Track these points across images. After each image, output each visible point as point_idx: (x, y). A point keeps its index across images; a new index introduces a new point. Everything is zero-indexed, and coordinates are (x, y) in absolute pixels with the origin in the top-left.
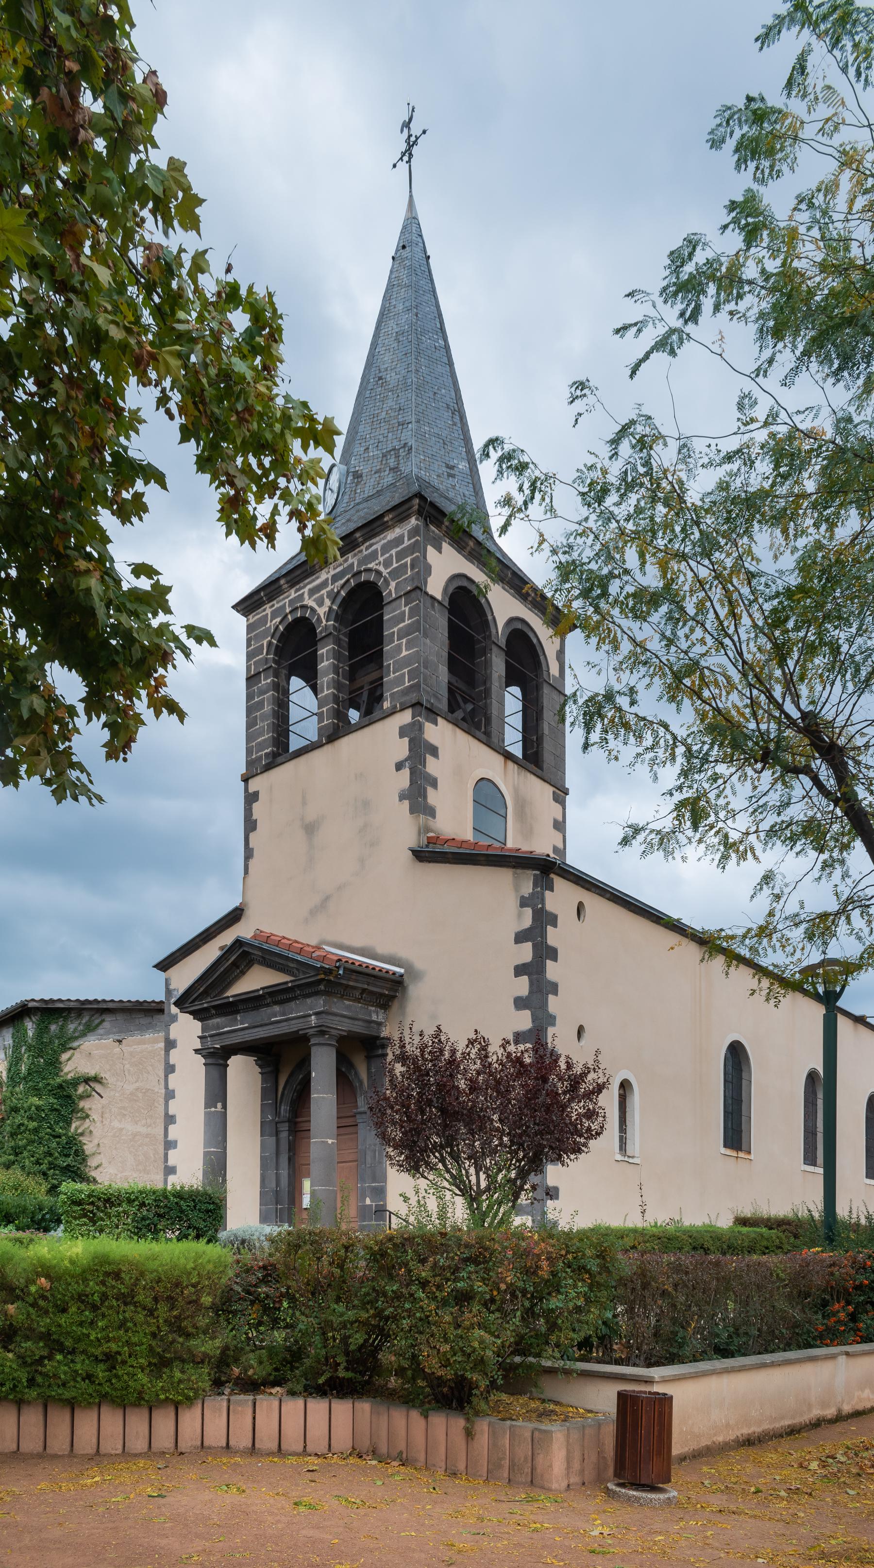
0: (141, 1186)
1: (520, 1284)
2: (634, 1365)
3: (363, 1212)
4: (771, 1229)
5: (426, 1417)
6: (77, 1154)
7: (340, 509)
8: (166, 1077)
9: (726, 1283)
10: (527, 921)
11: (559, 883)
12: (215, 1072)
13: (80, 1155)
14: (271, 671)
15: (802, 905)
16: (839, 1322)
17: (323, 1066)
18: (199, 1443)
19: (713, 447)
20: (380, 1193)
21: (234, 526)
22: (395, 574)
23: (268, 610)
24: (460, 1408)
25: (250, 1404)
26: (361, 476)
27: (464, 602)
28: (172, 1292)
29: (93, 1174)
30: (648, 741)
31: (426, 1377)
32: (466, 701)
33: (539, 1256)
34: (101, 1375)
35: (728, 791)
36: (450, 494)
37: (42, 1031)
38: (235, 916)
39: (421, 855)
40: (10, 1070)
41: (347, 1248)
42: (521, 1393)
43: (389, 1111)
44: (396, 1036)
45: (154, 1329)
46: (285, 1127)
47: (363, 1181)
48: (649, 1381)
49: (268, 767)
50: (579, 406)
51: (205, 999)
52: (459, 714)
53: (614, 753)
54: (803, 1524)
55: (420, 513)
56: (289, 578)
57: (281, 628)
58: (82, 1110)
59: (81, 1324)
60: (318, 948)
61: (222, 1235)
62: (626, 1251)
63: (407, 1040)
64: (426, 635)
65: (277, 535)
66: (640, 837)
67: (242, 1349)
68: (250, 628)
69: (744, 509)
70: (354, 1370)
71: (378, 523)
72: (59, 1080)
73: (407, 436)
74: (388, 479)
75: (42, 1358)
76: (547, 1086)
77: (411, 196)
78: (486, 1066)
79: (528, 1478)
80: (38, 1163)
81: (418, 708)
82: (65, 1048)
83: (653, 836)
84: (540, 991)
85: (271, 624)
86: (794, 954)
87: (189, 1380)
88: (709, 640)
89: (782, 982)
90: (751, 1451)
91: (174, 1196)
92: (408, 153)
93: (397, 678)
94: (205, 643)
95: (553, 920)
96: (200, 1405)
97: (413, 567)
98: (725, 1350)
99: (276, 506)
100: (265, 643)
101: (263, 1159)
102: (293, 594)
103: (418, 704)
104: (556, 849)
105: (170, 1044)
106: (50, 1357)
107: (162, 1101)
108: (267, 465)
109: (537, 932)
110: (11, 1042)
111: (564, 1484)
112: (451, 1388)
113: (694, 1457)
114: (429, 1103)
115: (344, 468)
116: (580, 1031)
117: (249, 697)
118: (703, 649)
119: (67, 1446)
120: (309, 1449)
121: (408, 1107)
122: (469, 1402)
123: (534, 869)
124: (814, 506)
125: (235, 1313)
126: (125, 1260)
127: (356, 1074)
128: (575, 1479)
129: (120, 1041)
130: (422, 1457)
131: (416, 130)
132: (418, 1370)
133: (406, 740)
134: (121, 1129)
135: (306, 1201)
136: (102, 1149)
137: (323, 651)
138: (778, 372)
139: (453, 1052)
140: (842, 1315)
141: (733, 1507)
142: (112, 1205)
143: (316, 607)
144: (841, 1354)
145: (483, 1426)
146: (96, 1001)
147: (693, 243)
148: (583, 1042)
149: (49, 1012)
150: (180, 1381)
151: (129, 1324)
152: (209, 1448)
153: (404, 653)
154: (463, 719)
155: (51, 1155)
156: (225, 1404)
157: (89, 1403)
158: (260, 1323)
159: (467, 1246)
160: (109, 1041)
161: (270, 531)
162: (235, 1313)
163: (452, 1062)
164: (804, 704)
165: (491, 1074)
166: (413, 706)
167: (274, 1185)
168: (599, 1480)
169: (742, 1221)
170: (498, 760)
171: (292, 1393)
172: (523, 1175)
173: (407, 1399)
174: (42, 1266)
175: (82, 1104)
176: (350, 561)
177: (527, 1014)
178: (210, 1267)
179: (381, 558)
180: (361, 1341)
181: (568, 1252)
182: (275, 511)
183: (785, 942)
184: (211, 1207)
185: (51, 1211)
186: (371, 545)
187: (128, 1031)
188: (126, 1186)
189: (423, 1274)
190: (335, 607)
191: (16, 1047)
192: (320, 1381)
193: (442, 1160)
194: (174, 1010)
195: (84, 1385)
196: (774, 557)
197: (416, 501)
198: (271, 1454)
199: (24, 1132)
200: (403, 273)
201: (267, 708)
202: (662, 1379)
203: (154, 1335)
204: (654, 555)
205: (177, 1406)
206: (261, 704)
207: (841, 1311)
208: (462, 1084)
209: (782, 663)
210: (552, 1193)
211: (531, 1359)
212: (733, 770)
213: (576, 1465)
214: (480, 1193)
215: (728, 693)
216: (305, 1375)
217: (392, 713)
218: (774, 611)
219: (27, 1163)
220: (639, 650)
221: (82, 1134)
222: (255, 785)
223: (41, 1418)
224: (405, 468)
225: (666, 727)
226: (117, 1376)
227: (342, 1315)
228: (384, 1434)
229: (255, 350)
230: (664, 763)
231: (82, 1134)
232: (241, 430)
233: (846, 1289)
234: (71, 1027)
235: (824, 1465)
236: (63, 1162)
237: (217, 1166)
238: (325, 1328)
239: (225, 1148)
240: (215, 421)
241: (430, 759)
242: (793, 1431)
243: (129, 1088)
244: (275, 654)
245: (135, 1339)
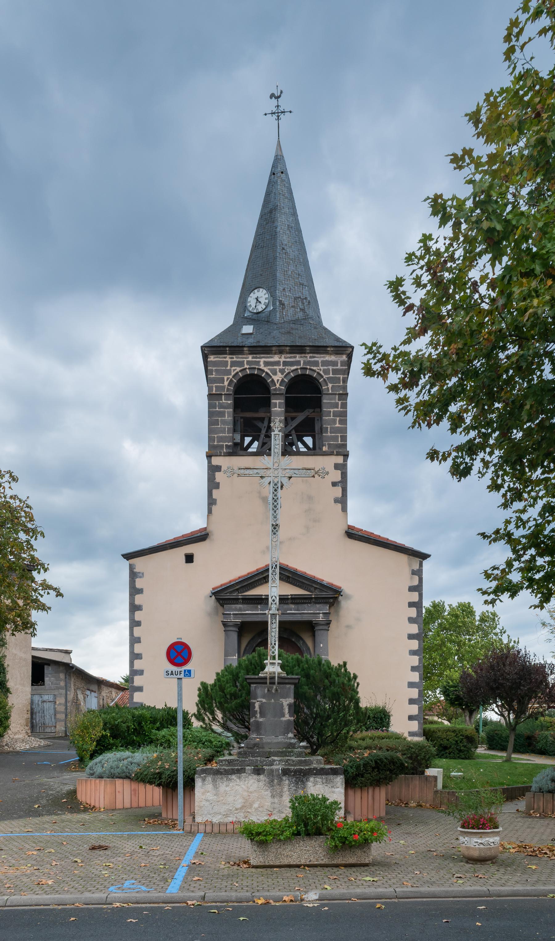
56: (251, 349)
71: (323, 349)
77: (279, 142)
127: (304, 642)
134: (16, 654)
176: (298, 359)
186: (314, 357)
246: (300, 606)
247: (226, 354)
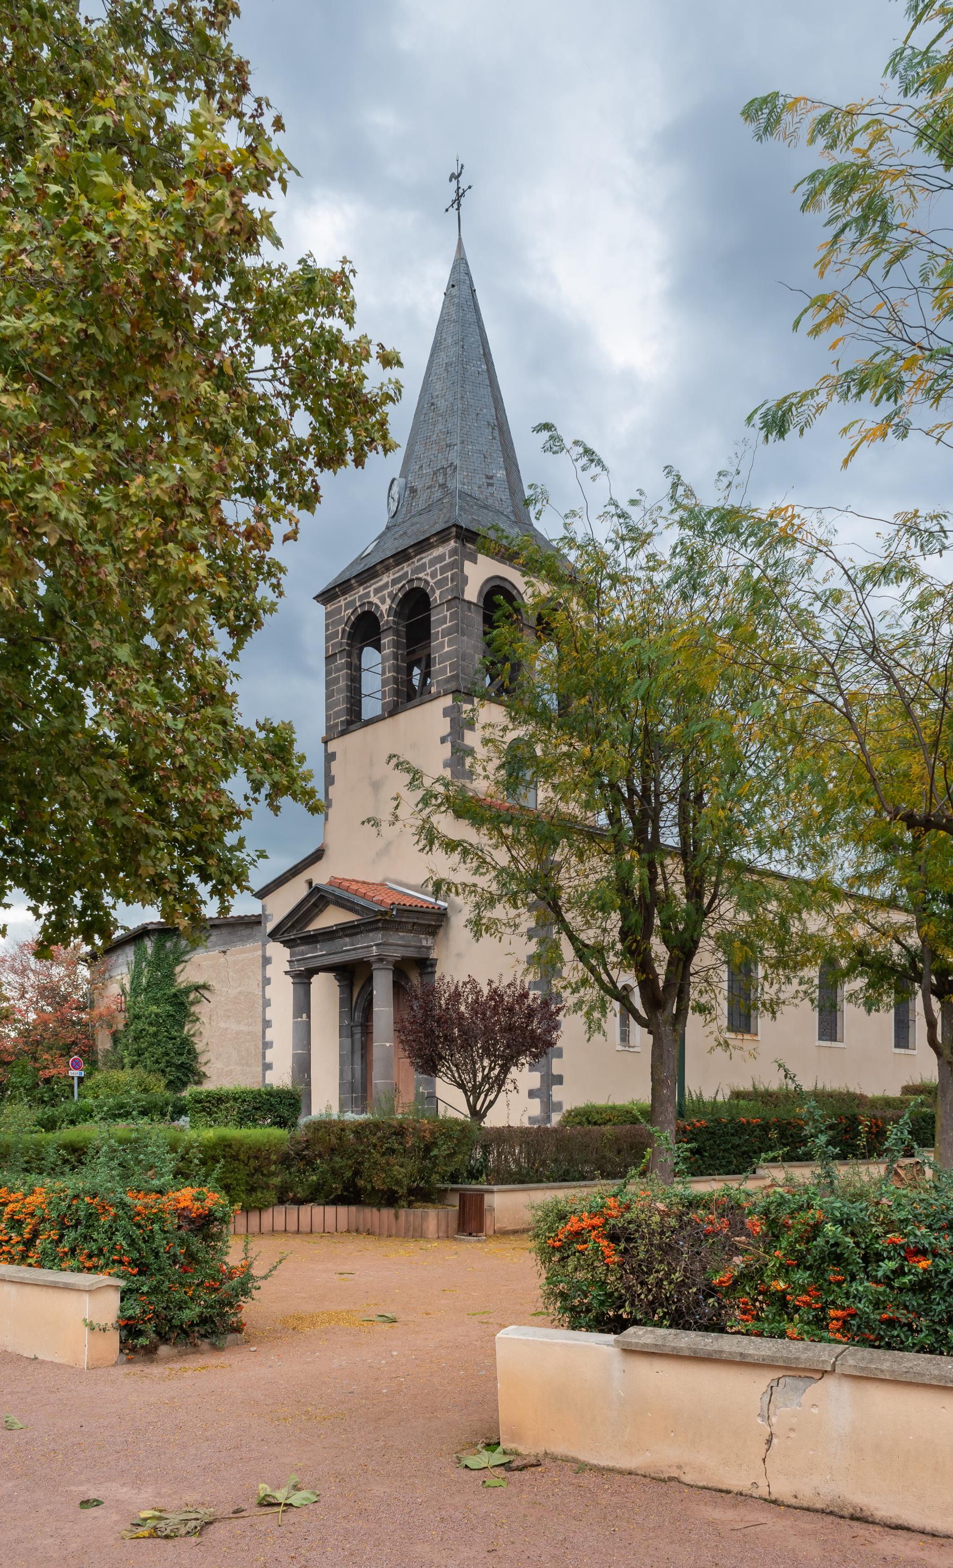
6: (189, 1052)
8: (263, 988)
12: (301, 989)
13: (193, 1054)
14: (345, 653)
22: (440, 584)
23: (342, 601)
26: (416, 491)
27: (497, 596)
29: (203, 1069)
37: (159, 948)
38: (318, 856)
40: (132, 982)
46: (358, 1030)
49: (343, 733)
55: (457, 537)
57: (353, 618)
58: (193, 1014)
64: (463, 634)
68: (328, 615)
72: (173, 990)
77: (460, 239)
80: (157, 1062)
81: (456, 694)
82: (178, 961)
93: (442, 669)
102: (361, 591)
117: (328, 673)
126: (234, 1139)
129: (224, 952)
136: (210, 1047)
155: (168, 1055)
160: (215, 953)
166: (453, 692)
167: (350, 1078)
169: (737, 1095)
175: (193, 1009)
179: (428, 570)
191: (138, 964)
197: (454, 529)
198: (307, 1233)
201: (342, 683)
205: (260, 1210)
206: (337, 680)
213: (443, 1227)
217: (438, 697)
221: (193, 1035)
222: (333, 746)
231: (193, 1035)
236: (178, 1060)
237: (303, 1066)
239: (309, 1050)
243: (233, 992)
247: (338, 596)
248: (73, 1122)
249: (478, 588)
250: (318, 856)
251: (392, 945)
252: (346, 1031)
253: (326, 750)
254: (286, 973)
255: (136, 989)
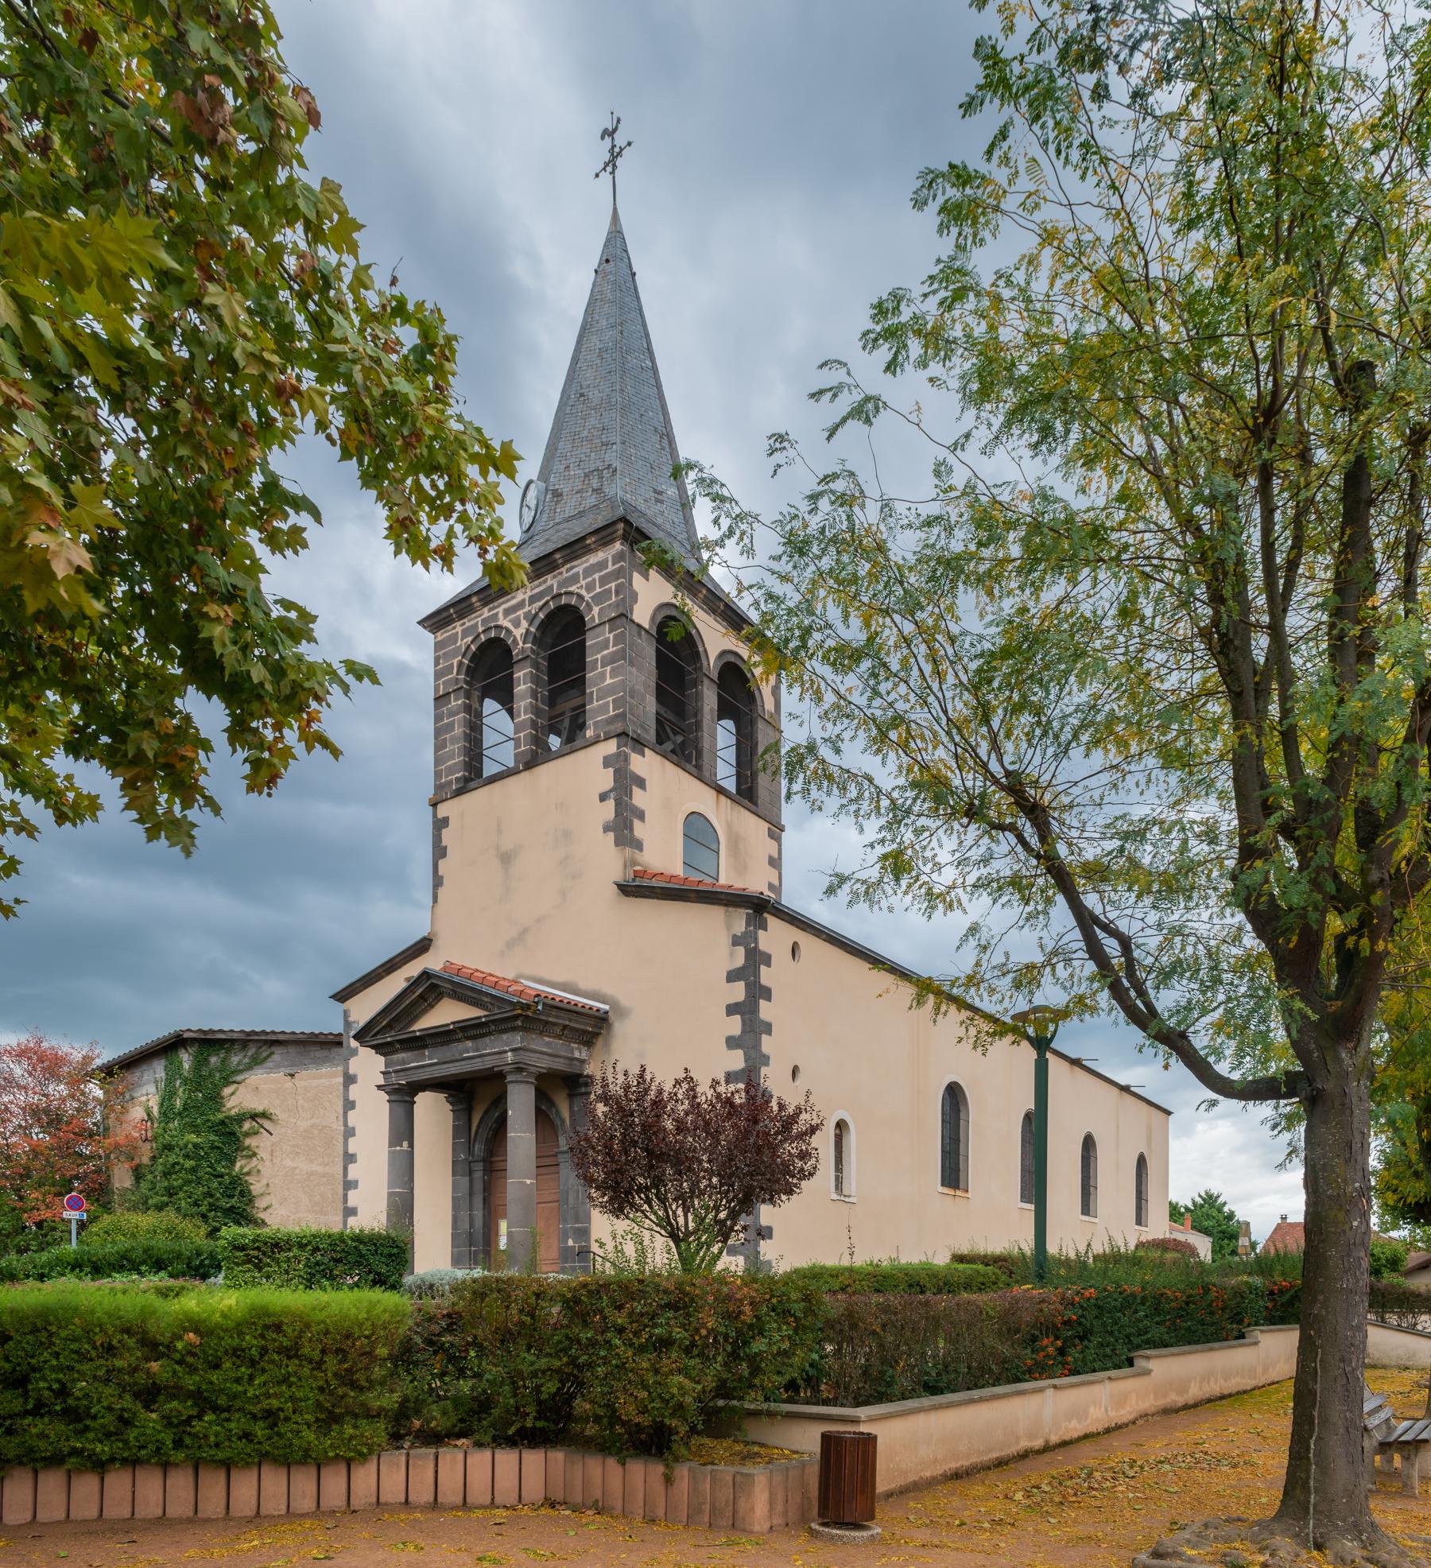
0: (314, 1229)
1: (722, 1329)
2: (842, 1405)
3: (565, 1254)
4: (987, 1265)
5: (624, 1464)
6: (242, 1194)
7: (538, 527)
9: (935, 1322)
10: (739, 960)
11: (772, 921)
12: (400, 1109)
13: (247, 1196)
14: (462, 693)
15: (1007, 955)
16: (1048, 1356)
17: (520, 1103)
18: (374, 1500)
19: (913, 511)
20: (584, 1233)
21: (405, 545)
22: (599, 599)
23: (458, 628)
24: (660, 1454)
25: (432, 1457)
28: (343, 1345)
29: (261, 1215)
30: (853, 792)
31: (624, 1424)
32: (675, 733)
33: (741, 1301)
34: (259, 1433)
35: (934, 844)
36: (658, 518)
37: (200, 1063)
38: (423, 946)
39: (627, 890)
41: (538, 1295)
42: (725, 1436)
43: (590, 1152)
44: (598, 1075)
45: (321, 1383)
46: (479, 1166)
47: (565, 1221)
48: (855, 1421)
49: (459, 792)
50: (779, 457)
51: (389, 1032)
52: (669, 746)
53: (818, 803)
54: (1004, 1554)
55: (625, 538)
57: (473, 648)
58: (248, 1148)
59: (238, 1380)
60: (516, 982)
61: (408, 1280)
62: (835, 1293)
63: (611, 1080)
64: (632, 664)
65: (455, 559)
66: (846, 888)
67: (424, 1400)
68: (438, 646)
69: (950, 569)
70: (547, 1419)
71: (580, 545)
72: (220, 1116)
73: (612, 457)
74: (591, 500)
75: (190, 1418)
76: (758, 1128)
77: (615, 209)
78: (695, 1106)
79: (729, 1521)
80: (196, 1204)
81: (624, 738)
83: (858, 885)
84: (753, 1031)
85: (462, 643)
86: (1008, 1003)
87: (362, 1435)
88: (912, 697)
89: (1000, 1028)
90: (958, 1484)
91: (353, 1240)
92: (611, 164)
94: (366, 680)
95: (767, 960)
96: (375, 1461)
97: (617, 593)
98: (934, 1387)
99: (451, 527)
100: (455, 662)
101: (455, 1201)
102: (486, 613)
103: (624, 734)
104: (771, 887)
105: (350, 1079)
106: (200, 1417)
107: (341, 1138)
108: (442, 487)
109: (751, 970)
110: (163, 1075)
111: (767, 1526)
112: (648, 1434)
113: (901, 1492)
114: (634, 1144)
115: (542, 485)
116: (795, 1071)
117: (438, 718)
118: (908, 706)
119: (221, 1509)
120: (497, 1501)
121: (611, 1149)
122: (669, 1448)
123: (747, 908)
124: (1019, 571)
125: (416, 1364)
126: (287, 1311)
127: (558, 1112)
128: (778, 1521)
129: (292, 1075)
130: (619, 1505)
131: (620, 139)
132: (614, 1418)
133: (611, 770)
135: (503, 1243)
136: (271, 1189)
137: (519, 674)
138: (974, 446)
139: (660, 1092)
140: (1051, 1350)
141: (936, 1541)
142: (281, 1250)
143: (511, 628)
144: (1049, 1387)
145: (682, 1472)
146: (264, 1032)
147: (897, 297)
148: (798, 1082)
149: (209, 1043)
150: (352, 1438)
151: (293, 1379)
152: (386, 1504)
153: (609, 681)
154: (673, 751)
155: (212, 1196)
156: (403, 1459)
157: (247, 1463)
158: (443, 1374)
159: (666, 1292)
160: (280, 1075)
161: (446, 555)
162: (416, 1364)
163: (658, 1104)
164: (1007, 759)
165: (699, 1115)
166: (618, 736)
168: (803, 1520)
169: (959, 1258)
170: (711, 794)
171: (479, 1445)
172: (734, 1215)
173: (603, 1447)
174: (190, 1320)
175: (248, 1142)
176: (549, 583)
177: (740, 1053)
178: (386, 1316)
179: (585, 581)
180: (554, 1390)
181: (772, 1296)
182: (451, 534)
183: (992, 991)
184: (395, 1251)
185: (212, 1256)
186: (572, 568)
187: (304, 1065)
188: (297, 1229)
189: (619, 1321)
190: (533, 629)
191: (169, 1081)
192: (510, 1432)
193: (648, 1201)
194: (354, 1044)
195: (241, 1444)
196: (975, 618)
197: (621, 525)
199: (180, 1171)
200: (607, 289)
201: (458, 730)
202: (869, 1420)
203: (321, 1389)
204: (858, 608)
205: (349, 1463)
207: (1049, 1345)
208: (669, 1124)
209: (986, 720)
210: (764, 1233)
211: (735, 1402)
212: (939, 823)
213: (780, 1507)
214: (688, 1234)
215: (935, 748)
216: (493, 1425)
218: (979, 671)
219: (183, 1204)
220: (842, 702)
221: (248, 1174)
222: (443, 810)
223: (191, 1479)
224: (610, 490)
225: (871, 780)
226: (279, 1434)
227: (532, 1364)
228: (578, 1482)
229: (424, 368)
230: (869, 815)
231: (248, 1174)
232: (408, 450)
233: (1054, 1325)
234: (235, 1059)
235: (1028, 1495)
236: (226, 1203)
237: (402, 1207)
238: (514, 1378)
239: (412, 1189)
240: (379, 439)
241: (636, 790)
242: (1000, 1463)
243: (303, 1125)
244: (467, 674)
245: (299, 1394)
246: (480, 1042)
248: (41, 1278)
249: (650, 612)
250: (423, 946)
251: (535, 1051)
252: (460, 1168)
253: (435, 815)
254: (379, 1087)
255: (167, 1113)
